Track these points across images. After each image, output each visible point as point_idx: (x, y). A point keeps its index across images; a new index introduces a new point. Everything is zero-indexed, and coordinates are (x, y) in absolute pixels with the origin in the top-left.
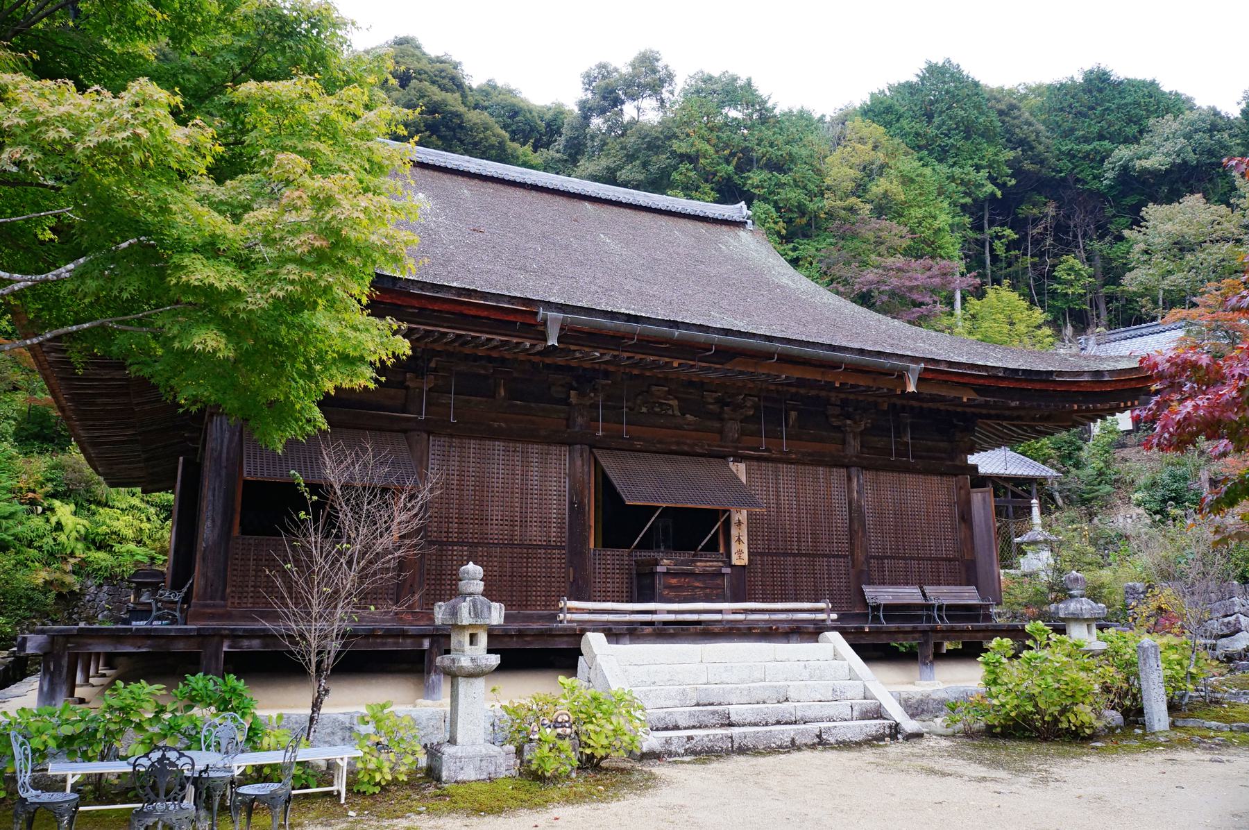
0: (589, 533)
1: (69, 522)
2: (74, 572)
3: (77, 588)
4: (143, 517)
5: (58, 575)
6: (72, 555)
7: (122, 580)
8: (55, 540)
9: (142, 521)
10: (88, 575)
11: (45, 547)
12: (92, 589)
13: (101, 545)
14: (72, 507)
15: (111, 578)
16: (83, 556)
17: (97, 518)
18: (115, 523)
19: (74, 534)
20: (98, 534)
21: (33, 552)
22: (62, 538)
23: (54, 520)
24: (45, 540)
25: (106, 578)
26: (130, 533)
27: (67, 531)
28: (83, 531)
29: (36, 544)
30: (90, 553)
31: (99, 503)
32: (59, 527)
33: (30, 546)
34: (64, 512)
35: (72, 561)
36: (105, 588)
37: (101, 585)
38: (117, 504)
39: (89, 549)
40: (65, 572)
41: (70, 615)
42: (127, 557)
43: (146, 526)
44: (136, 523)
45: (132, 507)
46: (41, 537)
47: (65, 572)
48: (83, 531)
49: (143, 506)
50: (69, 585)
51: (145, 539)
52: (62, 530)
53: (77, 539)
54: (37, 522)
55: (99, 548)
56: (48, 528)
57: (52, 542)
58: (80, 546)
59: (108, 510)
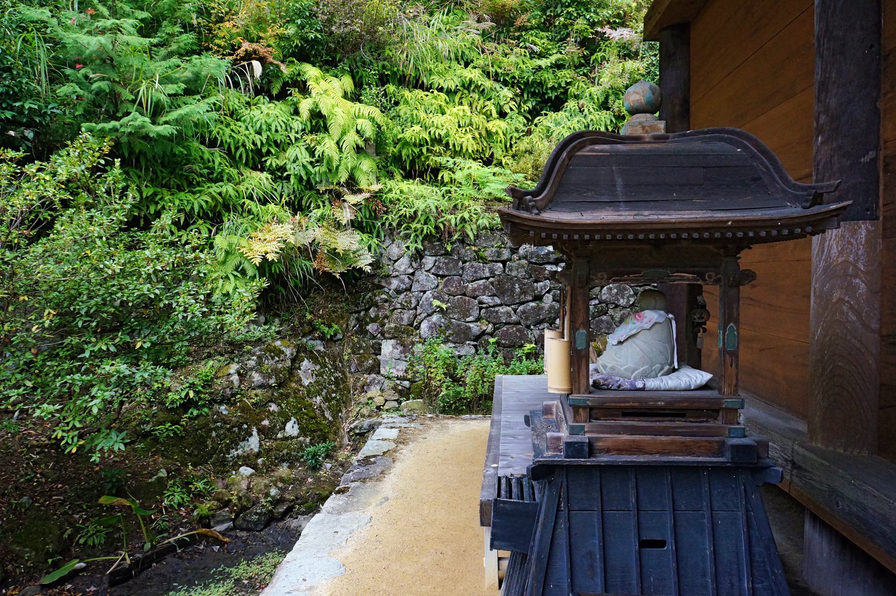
0: (686, 203)
1: (338, 111)
2: (356, 225)
3: (365, 262)
4: (491, 107)
5: (318, 233)
6: (352, 184)
7: (463, 240)
8: (311, 151)
9: (488, 116)
10: (391, 232)
11: (293, 170)
12: (403, 265)
13: (416, 168)
14: (347, 82)
15: (438, 239)
16: (376, 187)
17: (403, 109)
18: (438, 119)
19: (351, 139)
20: (406, 144)
21: (258, 180)
22: (327, 146)
23: (305, 106)
24: (291, 152)
25: (428, 237)
26: (468, 142)
27: (335, 131)
28: (369, 131)
29: (271, 162)
30: (390, 184)
31: (402, 81)
32: (319, 122)
33: (258, 167)
34: (327, 90)
35: (352, 199)
36: (429, 261)
37: (418, 256)
38: (436, 80)
39: (391, 176)
40: (338, 225)
41: (362, 324)
42: (469, 191)
43: (497, 125)
44: (479, 119)
45: (468, 86)
46: (282, 146)
47: (338, 225)
48: (369, 132)
49: (488, 83)
50: (344, 257)
51: (499, 154)
52: (326, 129)
53: (358, 150)
54: (268, 112)
55: (408, 176)
56: (297, 125)
57: (305, 158)
58: (367, 164)
59: (419, 93)
